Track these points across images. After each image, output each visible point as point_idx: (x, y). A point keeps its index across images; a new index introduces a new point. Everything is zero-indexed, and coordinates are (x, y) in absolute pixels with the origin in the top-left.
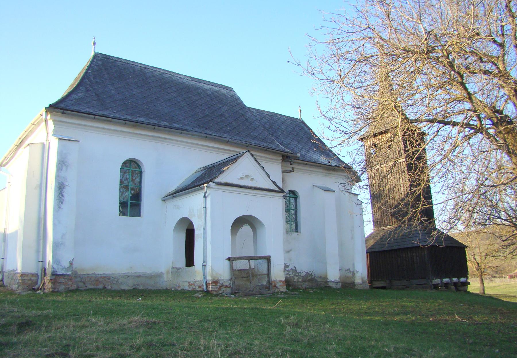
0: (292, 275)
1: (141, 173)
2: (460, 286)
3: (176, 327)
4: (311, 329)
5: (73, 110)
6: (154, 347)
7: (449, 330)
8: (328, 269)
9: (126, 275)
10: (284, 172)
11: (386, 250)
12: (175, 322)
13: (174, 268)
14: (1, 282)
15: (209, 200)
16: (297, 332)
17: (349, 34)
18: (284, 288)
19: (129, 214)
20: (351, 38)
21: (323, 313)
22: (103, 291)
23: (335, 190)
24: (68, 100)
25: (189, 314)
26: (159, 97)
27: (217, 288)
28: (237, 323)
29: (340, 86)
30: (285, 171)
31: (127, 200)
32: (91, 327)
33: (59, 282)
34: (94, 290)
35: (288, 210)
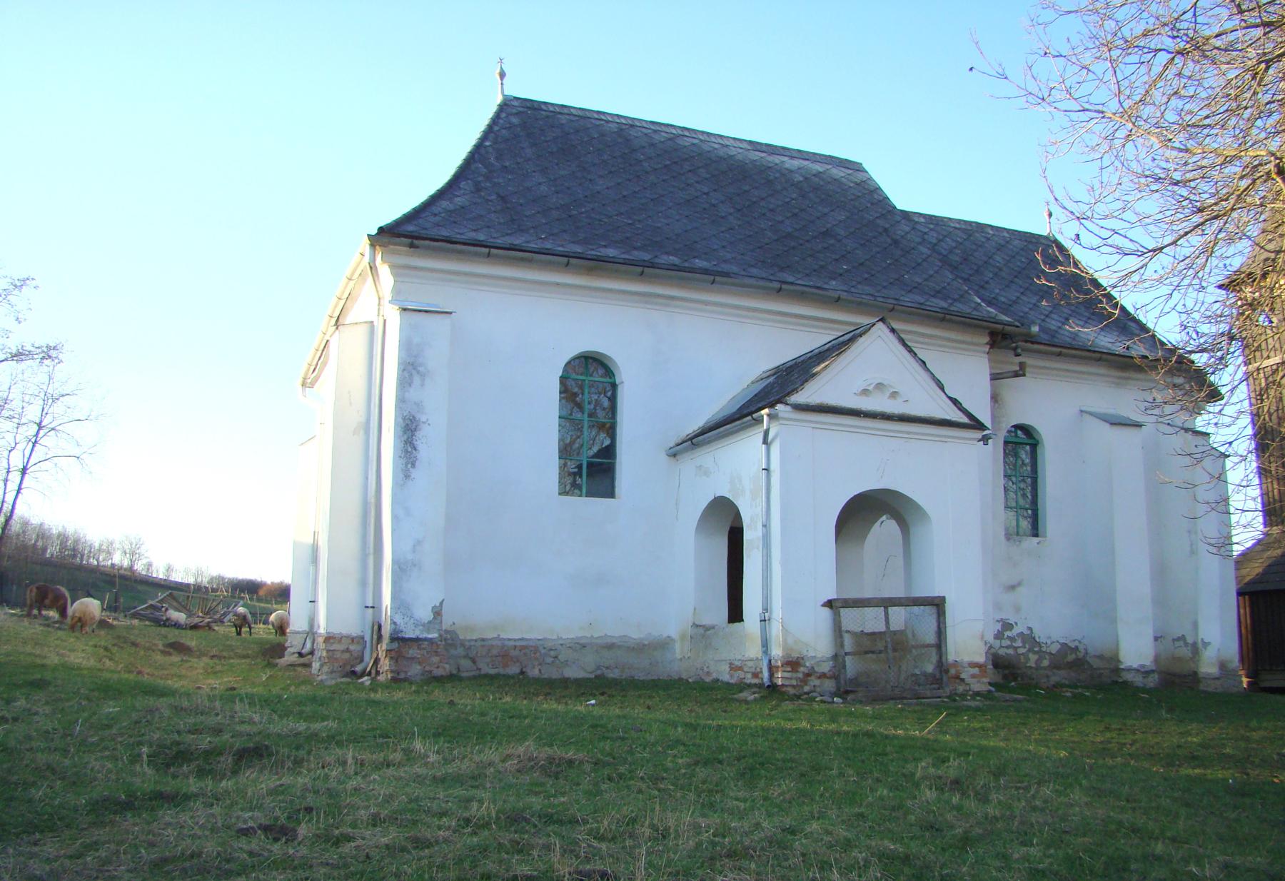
0: (1021, 651)
1: (614, 386)
5: (437, 237)
8: (1120, 633)
9: (578, 643)
10: (998, 376)
13: (697, 626)
15: (775, 449)
18: (983, 683)
24: (427, 213)
26: (663, 196)
27: (797, 679)
30: (998, 374)
33: (409, 656)
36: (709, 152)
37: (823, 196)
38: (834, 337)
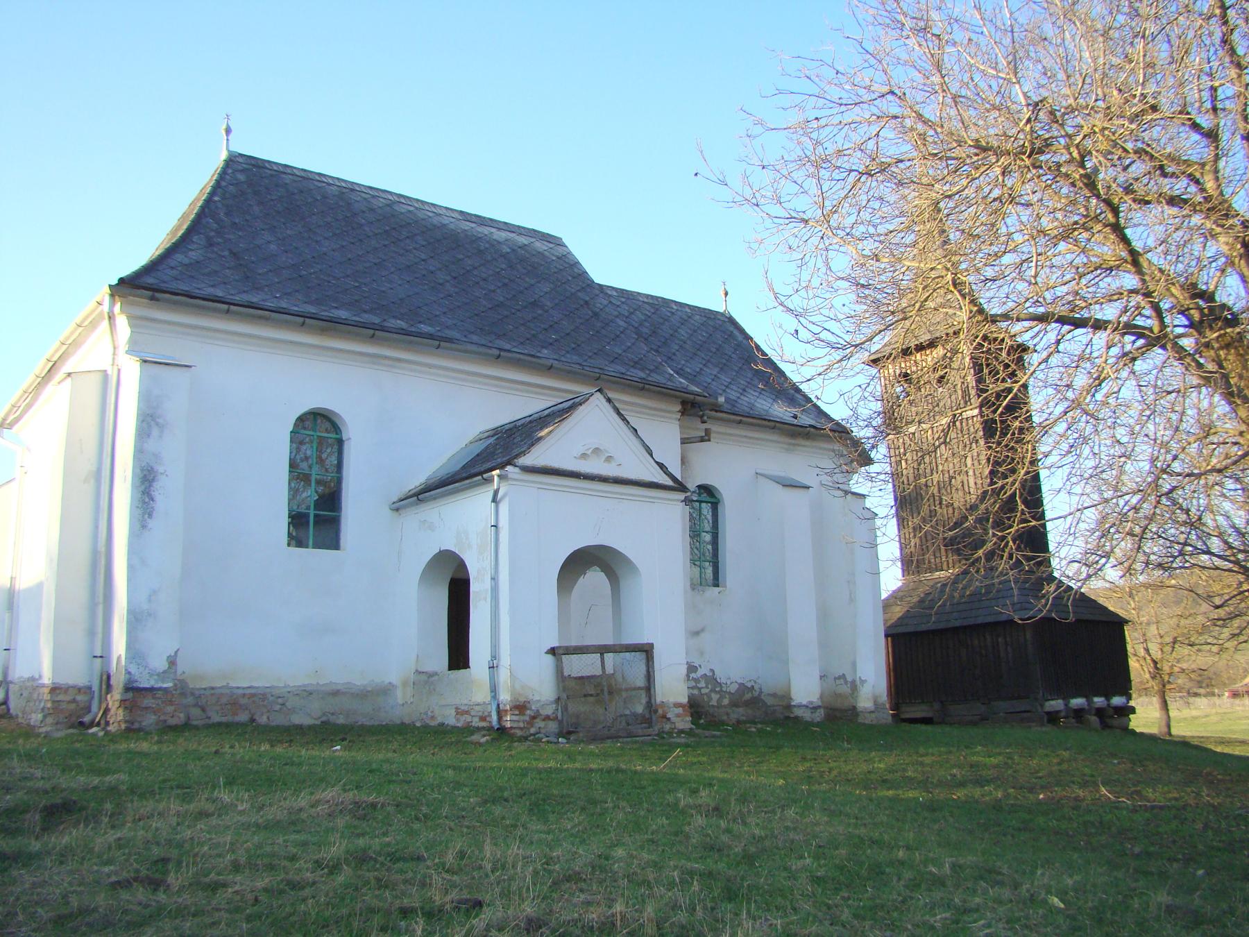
0: (704, 691)
1: (340, 442)
3: (425, 816)
4: (752, 820)
14: (4, 707)
15: (504, 508)
16: (718, 827)
17: (843, 108)
19: (311, 542)
20: (848, 118)
21: (781, 782)
22: (249, 729)
23: (809, 484)
25: (458, 785)
27: (524, 721)
29: (820, 234)
31: (308, 508)
32: (220, 816)
34: (228, 725)
35: (695, 534)
36: (423, 219)
37: (529, 268)
38: (554, 403)
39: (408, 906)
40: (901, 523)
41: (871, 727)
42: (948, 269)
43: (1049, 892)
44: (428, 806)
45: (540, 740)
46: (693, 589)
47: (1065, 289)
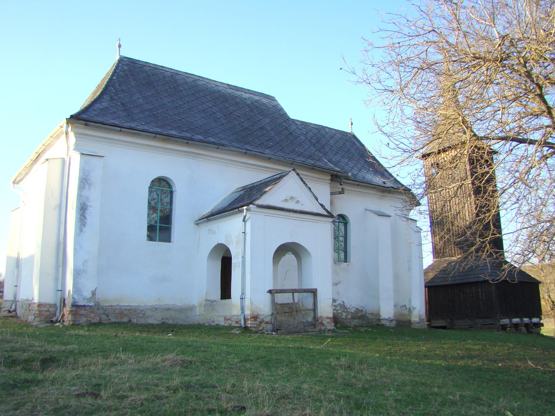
0: (339, 311)
1: (172, 193)
2: (532, 328)
3: (215, 367)
4: (365, 372)
6: (192, 388)
7: (521, 378)
8: (381, 304)
11: (452, 285)
12: (213, 362)
14: (14, 312)
15: (248, 224)
16: (350, 375)
17: (410, 38)
18: (332, 326)
19: (157, 239)
20: (412, 42)
21: (378, 355)
22: (129, 325)
23: (390, 214)
24: (91, 110)
25: (229, 353)
27: (256, 324)
28: (282, 364)
29: (399, 98)
31: (156, 222)
32: (121, 365)
34: (119, 323)
35: (336, 238)
37: (260, 111)
38: (272, 175)
39: (211, 408)
40: (433, 233)
41: (417, 330)
42: (459, 115)
43: (506, 409)
44: (215, 362)
45: (263, 333)
46: (335, 263)
47: (515, 124)
